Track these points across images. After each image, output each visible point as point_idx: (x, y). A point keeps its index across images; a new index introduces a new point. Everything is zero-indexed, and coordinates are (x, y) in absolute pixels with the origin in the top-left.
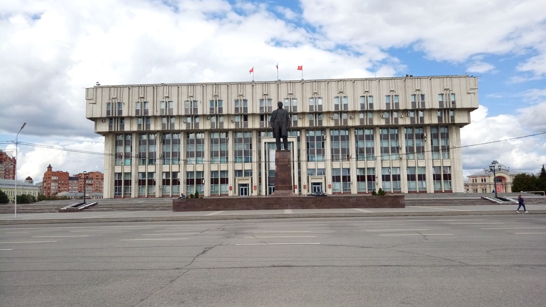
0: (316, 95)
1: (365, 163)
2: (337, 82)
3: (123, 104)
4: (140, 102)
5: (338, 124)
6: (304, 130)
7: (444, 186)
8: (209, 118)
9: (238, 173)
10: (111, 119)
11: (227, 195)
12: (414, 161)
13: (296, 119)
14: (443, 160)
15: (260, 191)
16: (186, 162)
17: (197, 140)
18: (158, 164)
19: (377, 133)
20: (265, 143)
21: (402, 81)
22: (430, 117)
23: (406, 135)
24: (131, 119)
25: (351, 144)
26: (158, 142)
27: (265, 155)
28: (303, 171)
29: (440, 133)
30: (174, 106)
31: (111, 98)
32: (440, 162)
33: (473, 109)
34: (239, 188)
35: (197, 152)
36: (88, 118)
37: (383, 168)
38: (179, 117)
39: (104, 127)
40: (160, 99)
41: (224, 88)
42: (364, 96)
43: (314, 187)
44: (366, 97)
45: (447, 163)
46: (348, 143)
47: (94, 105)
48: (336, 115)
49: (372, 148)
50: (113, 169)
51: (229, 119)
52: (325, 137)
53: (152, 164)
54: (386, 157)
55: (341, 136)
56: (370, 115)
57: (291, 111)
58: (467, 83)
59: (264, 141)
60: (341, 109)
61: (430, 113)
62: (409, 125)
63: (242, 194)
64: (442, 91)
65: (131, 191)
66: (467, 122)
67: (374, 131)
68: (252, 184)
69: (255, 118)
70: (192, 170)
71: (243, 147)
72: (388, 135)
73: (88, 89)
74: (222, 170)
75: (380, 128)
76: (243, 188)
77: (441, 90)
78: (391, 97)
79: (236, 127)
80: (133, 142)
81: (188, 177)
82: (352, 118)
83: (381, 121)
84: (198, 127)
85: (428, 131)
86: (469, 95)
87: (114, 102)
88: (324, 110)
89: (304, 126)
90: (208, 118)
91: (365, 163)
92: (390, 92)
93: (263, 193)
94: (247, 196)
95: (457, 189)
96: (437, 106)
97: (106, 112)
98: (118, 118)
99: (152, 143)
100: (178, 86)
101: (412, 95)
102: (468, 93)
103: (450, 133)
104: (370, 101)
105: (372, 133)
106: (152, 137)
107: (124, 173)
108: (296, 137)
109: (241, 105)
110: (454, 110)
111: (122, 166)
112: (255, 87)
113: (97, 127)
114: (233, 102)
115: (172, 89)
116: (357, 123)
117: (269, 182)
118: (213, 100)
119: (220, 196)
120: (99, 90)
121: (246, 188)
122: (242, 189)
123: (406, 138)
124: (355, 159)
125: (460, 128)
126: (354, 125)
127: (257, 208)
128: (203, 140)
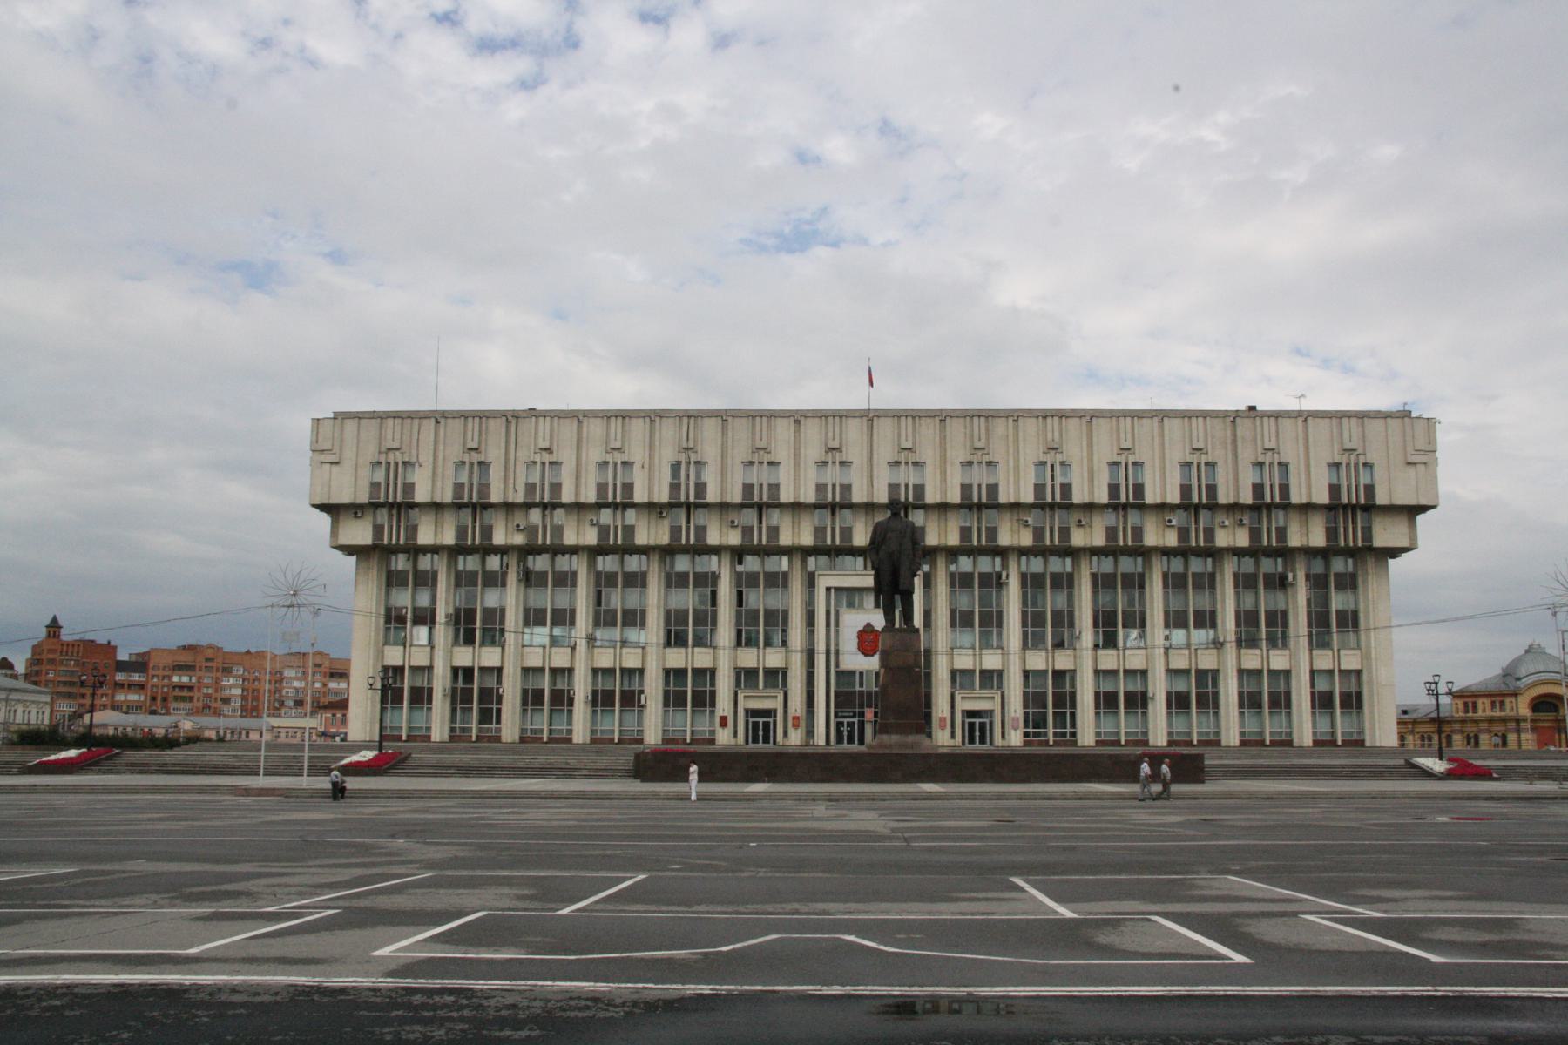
1: (1118, 655)
3: (417, 465)
5: (971, 541)
6: (944, 555)
7: (1342, 725)
8: (664, 514)
9: (746, 677)
11: (712, 741)
12: (1187, 652)
13: (774, 522)
14: (1339, 650)
15: (810, 732)
17: (485, 572)
19: (1155, 569)
20: (828, 589)
21: (1224, 423)
22: (942, 525)
23: (1236, 576)
24: (721, 515)
25: (1080, 600)
26: (512, 578)
27: (828, 625)
28: (940, 677)
29: (1332, 574)
30: (711, 478)
31: (383, 449)
33: (1424, 509)
36: (314, 506)
38: (578, 507)
39: (360, 533)
40: (524, 455)
41: (710, 428)
42: (606, 463)
43: (753, 722)
44: (1123, 465)
45: (1350, 661)
46: (1213, 594)
47: (335, 468)
50: (380, 654)
52: (1004, 576)
53: (493, 643)
54: (1179, 636)
55: (1336, 575)
56: (1133, 518)
57: (907, 498)
58: (1404, 436)
59: (823, 582)
60: (1053, 498)
61: (1304, 518)
62: (1174, 548)
63: (755, 740)
64: (1041, 455)
66: (1405, 544)
67: (1147, 564)
68: (786, 712)
70: (1042, 666)
71: (687, 599)
72: (1326, 576)
73: (317, 422)
74: (554, 665)
75: (1234, 555)
77: (1256, 449)
79: (743, 541)
81: (1243, 686)
82: (1083, 523)
83: (1021, 532)
84: (633, 540)
86: (1411, 470)
87: (392, 460)
88: (1002, 499)
89: (943, 542)
90: (661, 513)
91: (1118, 655)
92: (973, 452)
93: (820, 739)
94: (771, 745)
95: (1377, 737)
96: (1323, 498)
99: (495, 580)
100: (578, 417)
102: (1409, 464)
103: (1360, 573)
107: (410, 667)
112: (730, 427)
113: (340, 531)
114: (593, 468)
115: (520, 425)
116: (1099, 540)
117: (835, 707)
119: (689, 744)
122: (756, 725)
123: (1236, 586)
124: (1234, 644)
125: (1391, 561)
126: (1088, 544)
127: (848, 778)
128: (785, 575)
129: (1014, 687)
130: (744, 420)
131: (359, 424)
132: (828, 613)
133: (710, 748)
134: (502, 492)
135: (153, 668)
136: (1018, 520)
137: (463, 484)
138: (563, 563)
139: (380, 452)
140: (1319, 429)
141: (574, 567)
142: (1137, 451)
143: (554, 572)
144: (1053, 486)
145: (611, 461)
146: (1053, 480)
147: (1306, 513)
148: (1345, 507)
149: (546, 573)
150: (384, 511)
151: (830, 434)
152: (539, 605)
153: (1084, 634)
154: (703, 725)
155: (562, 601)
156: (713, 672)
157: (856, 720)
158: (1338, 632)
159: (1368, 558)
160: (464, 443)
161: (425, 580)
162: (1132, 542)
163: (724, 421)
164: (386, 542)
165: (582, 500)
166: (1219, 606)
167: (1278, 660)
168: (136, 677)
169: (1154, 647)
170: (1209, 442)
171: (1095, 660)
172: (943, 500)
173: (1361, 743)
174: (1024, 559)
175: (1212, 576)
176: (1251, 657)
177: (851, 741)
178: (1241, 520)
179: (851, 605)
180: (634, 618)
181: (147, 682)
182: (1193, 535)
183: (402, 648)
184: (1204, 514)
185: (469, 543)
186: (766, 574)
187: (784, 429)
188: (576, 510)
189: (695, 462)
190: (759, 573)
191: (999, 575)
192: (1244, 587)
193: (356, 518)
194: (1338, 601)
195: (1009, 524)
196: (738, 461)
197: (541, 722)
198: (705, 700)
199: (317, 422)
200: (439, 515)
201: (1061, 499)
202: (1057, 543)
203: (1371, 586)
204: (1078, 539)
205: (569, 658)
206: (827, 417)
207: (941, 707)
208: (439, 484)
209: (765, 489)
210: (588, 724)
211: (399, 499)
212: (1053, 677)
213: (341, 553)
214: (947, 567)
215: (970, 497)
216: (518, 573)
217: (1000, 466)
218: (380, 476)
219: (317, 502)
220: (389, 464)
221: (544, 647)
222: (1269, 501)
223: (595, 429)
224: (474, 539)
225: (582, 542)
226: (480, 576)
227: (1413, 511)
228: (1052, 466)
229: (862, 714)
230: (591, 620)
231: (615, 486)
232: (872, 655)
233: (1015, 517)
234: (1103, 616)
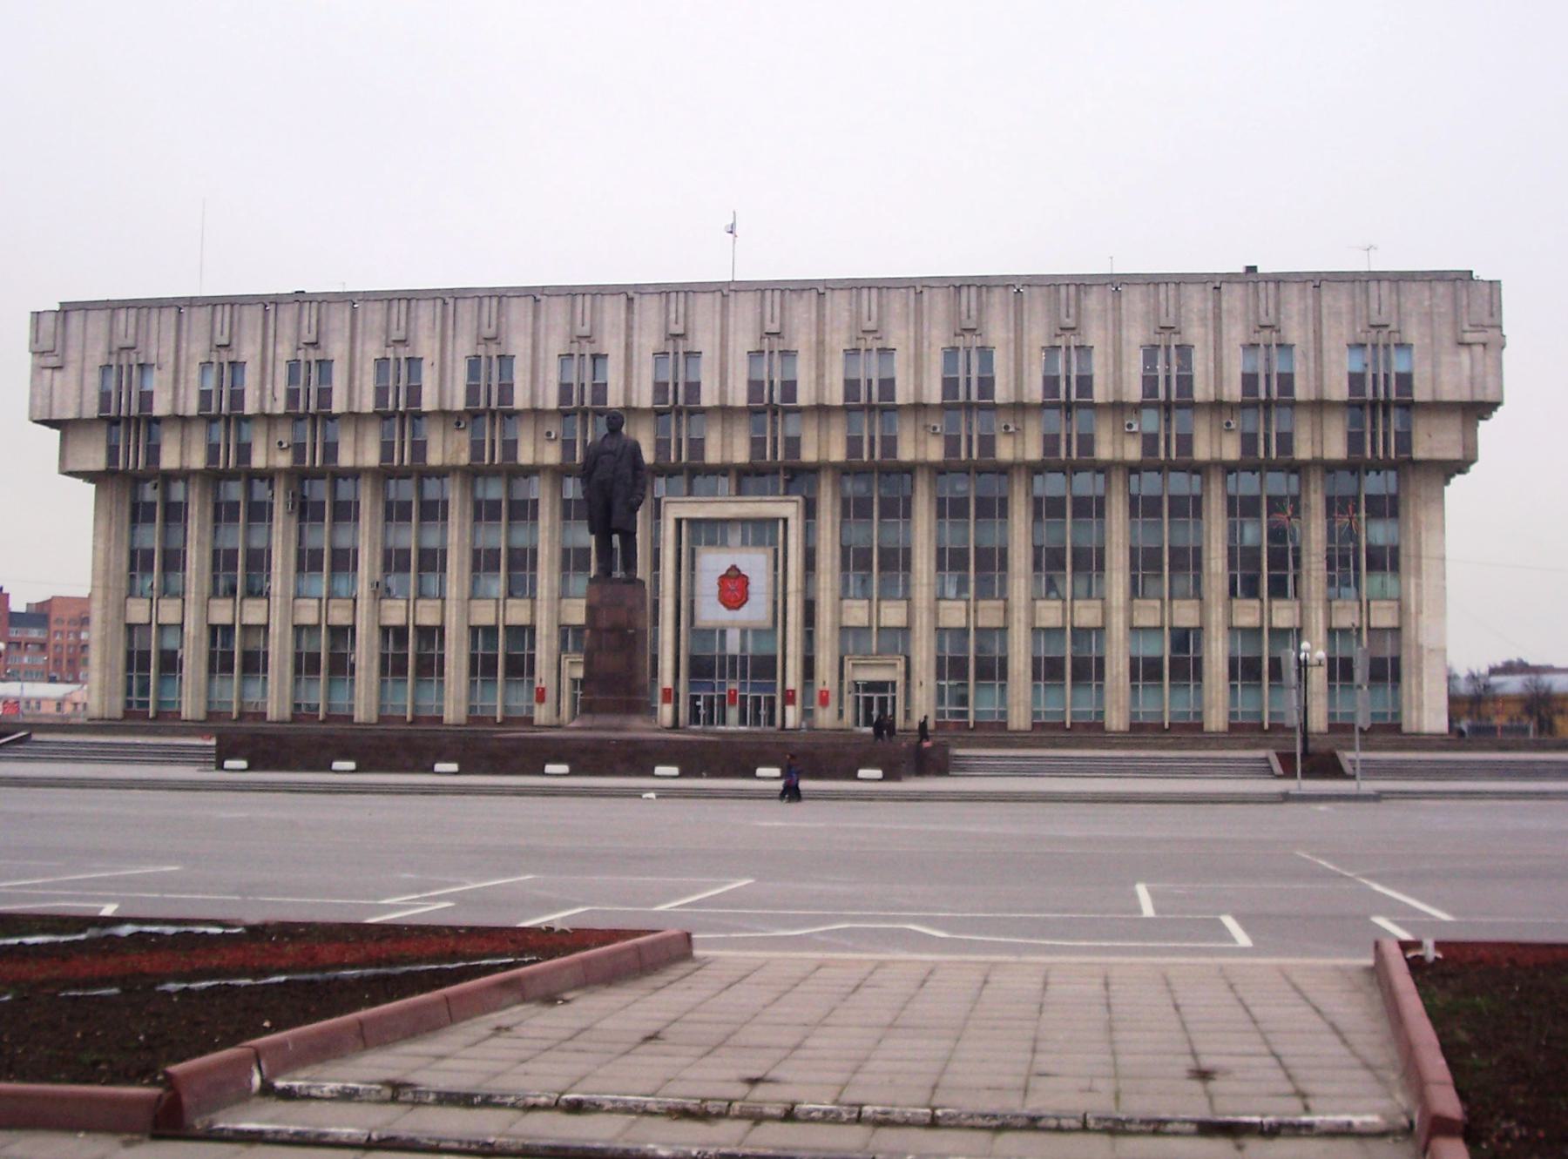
0: (870, 337)
2: (951, 288)
4: (114, 368)
8: (462, 426)
10: (114, 422)
11: (529, 721)
16: (382, 592)
18: (278, 592)
30: (614, 378)
31: (115, 349)
32: (1357, 608)
34: (858, 698)
35: (510, 550)
37: (1134, 629)
43: (741, 696)
45: (1383, 617)
46: (1198, 526)
47: (58, 375)
48: (1250, 414)
49: (747, 544)
51: (921, 424)
59: (672, 512)
65: (180, 695)
66: (1455, 454)
67: (1304, 483)
69: (275, 428)
73: (37, 316)
78: (1262, 351)
80: (450, 510)
82: (1011, 429)
85: (1312, 486)
87: (124, 362)
90: (458, 424)
97: (97, 400)
98: (138, 420)
104: (1399, 364)
105: (1392, 490)
106: (261, 491)
107: (507, 627)
108: (797, 501)
109: (869, 370)
111: (152, 599)
114: (554, 364)
115: (280, 314)
118: (479, 353)
120: (75, 319)
121: (886, 698)
122: (869, 701)
129: (923, 653)
130: (750, 295)
135: (57, 621)
136: (926, 427)
137: (211, 391)
139: (110, 353)
140: (1336, 301)
148: (1374, 405)
150: (307, 426)
151: (673, 316)
154: (520, 700)
156: (532, 629)
160: (212, 339)
163: (819, 294)
164: (121, 467)
166: (1205, 542)
167: (254, 613)
168: (34, 633)
172: (1118, 399)
173: (1396, 728)
178: (1228, 424)
179: (711, 543)
181: (48, 639)
182: (1162, 444)
188: (178, 429)
189: (1076, 347)
193: (458, 429)
194: (1378, 533)
198: (520, 667)
199: (37, 316)
200: (187, 431)
201: (980, 398)
203: (1417, 512)
204: (1005, 451)
205: (351, 612)
206: (668, 293)
211: (135, 411)
212: (241, 632)
213: (80, 481)
219: (35, 418)
220: (121, 367)
221: (320, 599)
222: (1263, 396)
231: (1068, 379)
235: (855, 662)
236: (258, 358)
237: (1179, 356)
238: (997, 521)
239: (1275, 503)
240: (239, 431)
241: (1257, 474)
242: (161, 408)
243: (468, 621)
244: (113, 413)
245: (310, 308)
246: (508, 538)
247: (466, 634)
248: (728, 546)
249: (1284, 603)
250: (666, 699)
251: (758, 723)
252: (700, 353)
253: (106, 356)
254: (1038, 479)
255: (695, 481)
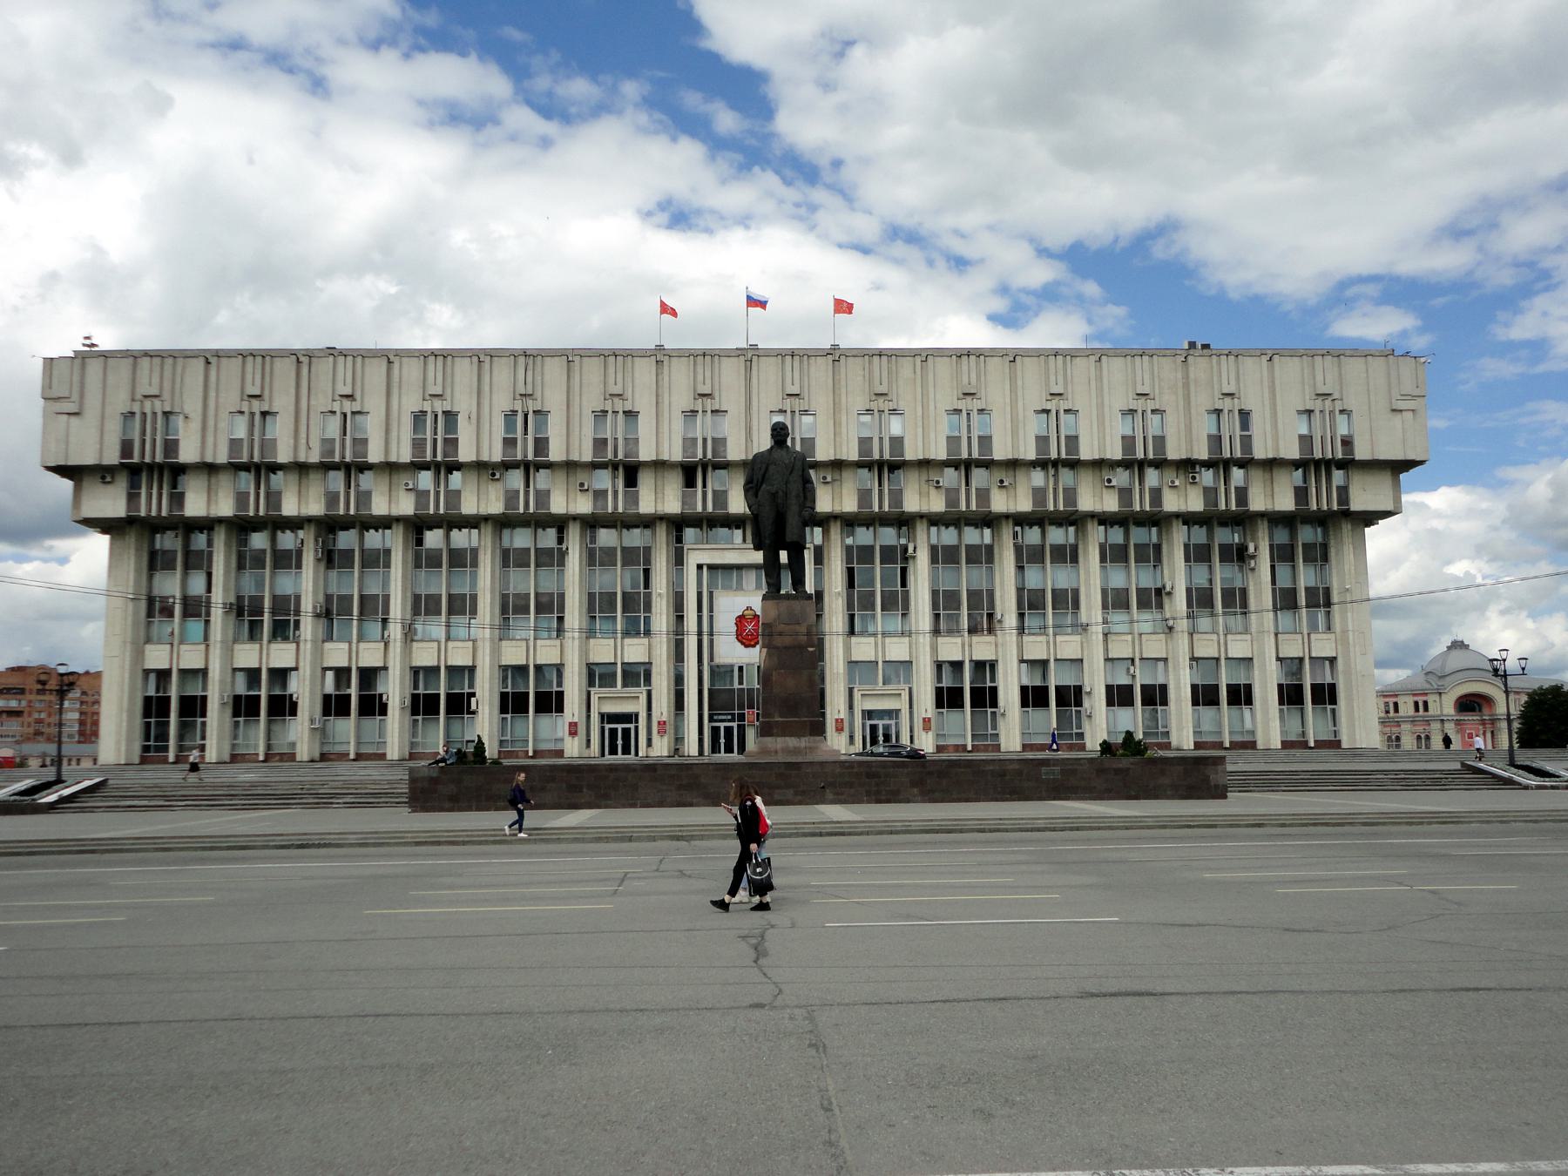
1: (1048, 642)
6: (839, 523)
7: (1314, 724)
8: (497, 476)
9: (597, 675)
11: (560, 753)
14: (1309, 634)
15: (679, 740)
19: (1090, 539)
20: (700, 567)
21: (1175, 362)
26: (309, 558)
27: (700, 609)
29: (1300, 544)
31: (139, 397)
33: (1408, 465)
35: (450, 596)
39: (111, 502)
40: (321, 402)
41: (554, 371)
43: (610, 729)
45: (1323, 646)
46: (991, 571)
47: (74, 420)
50: (139, 654)
52: (910, 550)
53: (286, 639)
59: (693, 559)
60: (970, 454)
61: (1267, 476)
62: (1200, 513)
65: (203, 738)
66: (1390, 507)
68: (649, 716)
71: (619, 580)
73: (49, 363)
76: (617, 729)
80: (215, 558)
86: (1398, 418)
87: (148, 410)
90: (493, 475)
91: (1048, 642)
92: (1049, 398)
93: (691, 747)
96: (1293, 453)
99: (286, 560)
101: (1209, 412)
105: (1072, 540)
110: (1347, 464)
116: (1025, 505)
119: (532, 757)
120: (94, 367)
122: (613, 732)
131: (105, 363)
132: (700, 595)
133: (1081, 755)
134: (291, 449)
138: (374, 539)
139: (133, 400)
141: (388, 545)
142: (1070, 397)
143: (362, 551)
144: (969, 438)
145: (429, 410)
146: (969, 431)
147: (1271, 470)
149: (529, 549)
152: (521, 589)
153: (1006, 617)
155: (549, 585)
157: (735, 725)
158: (1224, 614)
159: (1344, 526)
161: (196, 561)
162: (1150, 507)
165: (393, 459)
169: (917, 633)
170: (1157, 387)
171: (934, 649)
174: (934, 529)
175: (1158, 548)
176: (1205, 642)
177: (729, 749)
179: (727, 587)
180: (462, 605)
183: (168, 646)
184: (1237, 475)
185: (251, 514)
186: (624, 549)
187: (644, 371)
188: (830, 468)
190: (615, 549)
191: (905, 549)
192: (1195, 561)
193: (104, 483)
195: (917, 487)
196: (1202, 410)
197: (346, 729)
201: (1066, 455)
202: (1148, 509)
203: (1342, 555)
204: (1000, 503)
207: (836, 706)
208: (210, 440)
209: (709, 442)
210: (407, 736)
211: (159, 458)
214: (843, 541)
215: (870, 452)
216: (316, 551)
217: (1080, 414)
218: (241, 432)
223: (412, 370)
224: (257, 509)
225: (395, 512)
226: (357, 554)
227: (1399, 467)
228: (526, 416)
229: (742, 717)
230: (409, 607)
232: (754, 646)
233: (924, 477)
234: (337, 599)
235: (863, 692)
236: (292, 408)
237: (446, 422)
238: (984, 565)
239: (888, 554)
240: (268, 481)
241: (871, 529)
242: (188, 453)
243: (232, 664)
244: (136, 459)
245: (444, 364)
246: (449, 586)
247: (497, 674)
248: (742, 589)
249: (635, 641)
250: (839, 729)
251: (729, 749)
252: (726, 411)
253: (129, 403)
254: (506, 533)
255: (452, 533)
